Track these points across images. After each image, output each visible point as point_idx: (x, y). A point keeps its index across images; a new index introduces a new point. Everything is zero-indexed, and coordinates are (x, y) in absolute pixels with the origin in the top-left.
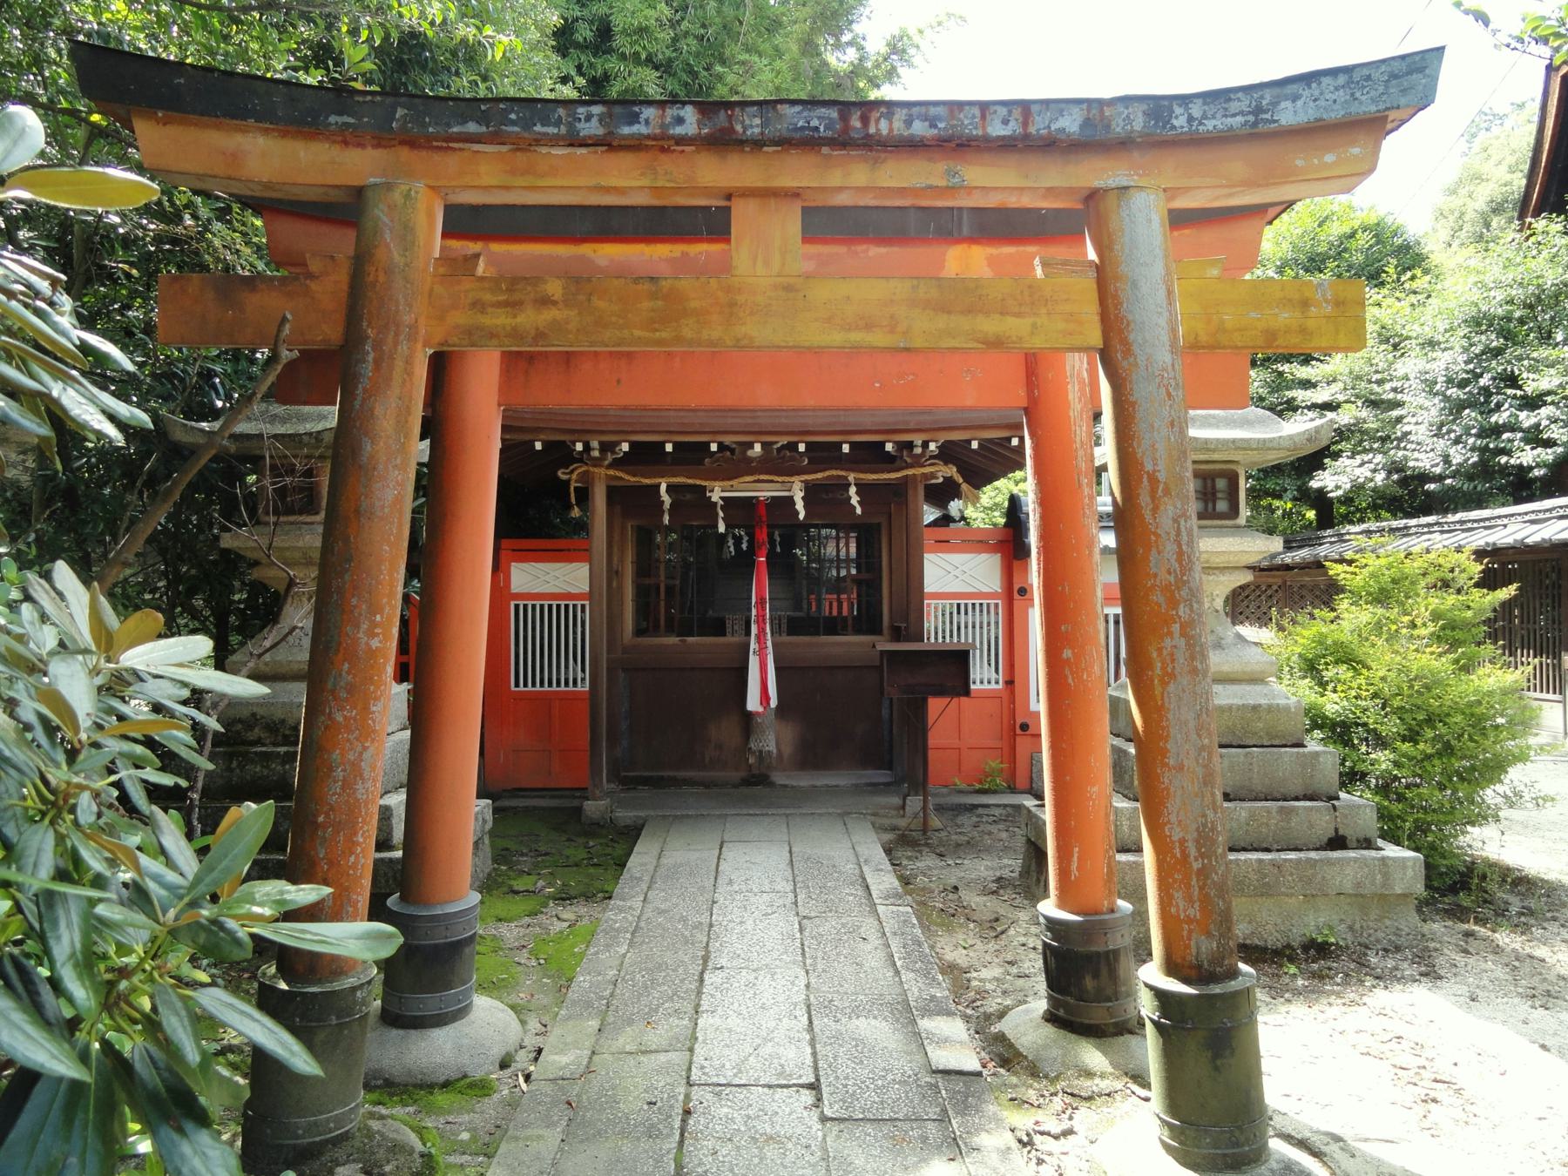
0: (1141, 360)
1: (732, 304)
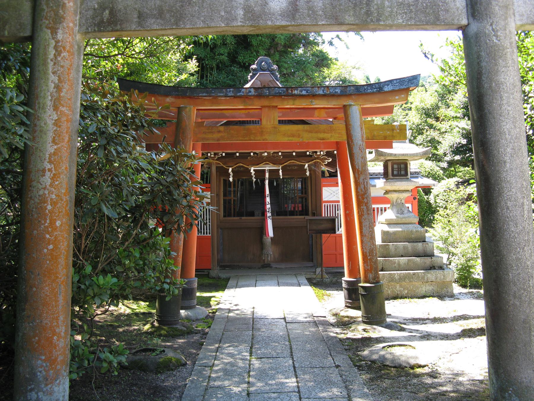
0: (355, 144)
1: (262, 132)
